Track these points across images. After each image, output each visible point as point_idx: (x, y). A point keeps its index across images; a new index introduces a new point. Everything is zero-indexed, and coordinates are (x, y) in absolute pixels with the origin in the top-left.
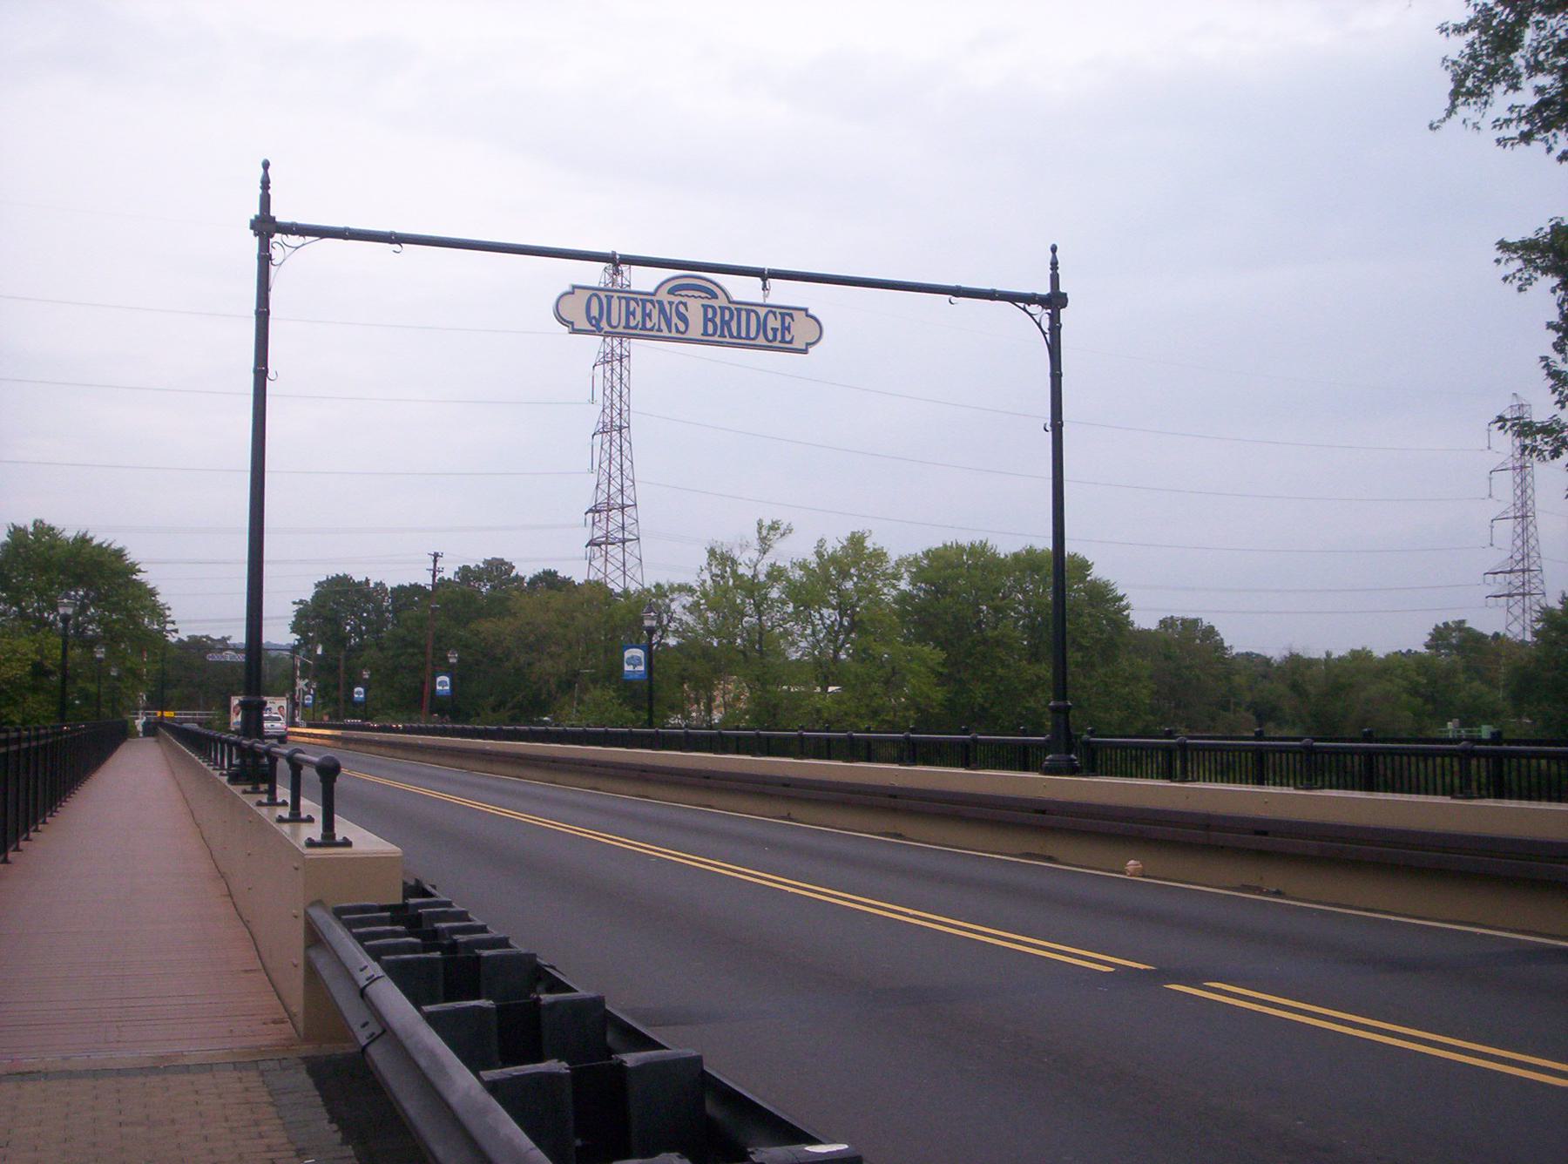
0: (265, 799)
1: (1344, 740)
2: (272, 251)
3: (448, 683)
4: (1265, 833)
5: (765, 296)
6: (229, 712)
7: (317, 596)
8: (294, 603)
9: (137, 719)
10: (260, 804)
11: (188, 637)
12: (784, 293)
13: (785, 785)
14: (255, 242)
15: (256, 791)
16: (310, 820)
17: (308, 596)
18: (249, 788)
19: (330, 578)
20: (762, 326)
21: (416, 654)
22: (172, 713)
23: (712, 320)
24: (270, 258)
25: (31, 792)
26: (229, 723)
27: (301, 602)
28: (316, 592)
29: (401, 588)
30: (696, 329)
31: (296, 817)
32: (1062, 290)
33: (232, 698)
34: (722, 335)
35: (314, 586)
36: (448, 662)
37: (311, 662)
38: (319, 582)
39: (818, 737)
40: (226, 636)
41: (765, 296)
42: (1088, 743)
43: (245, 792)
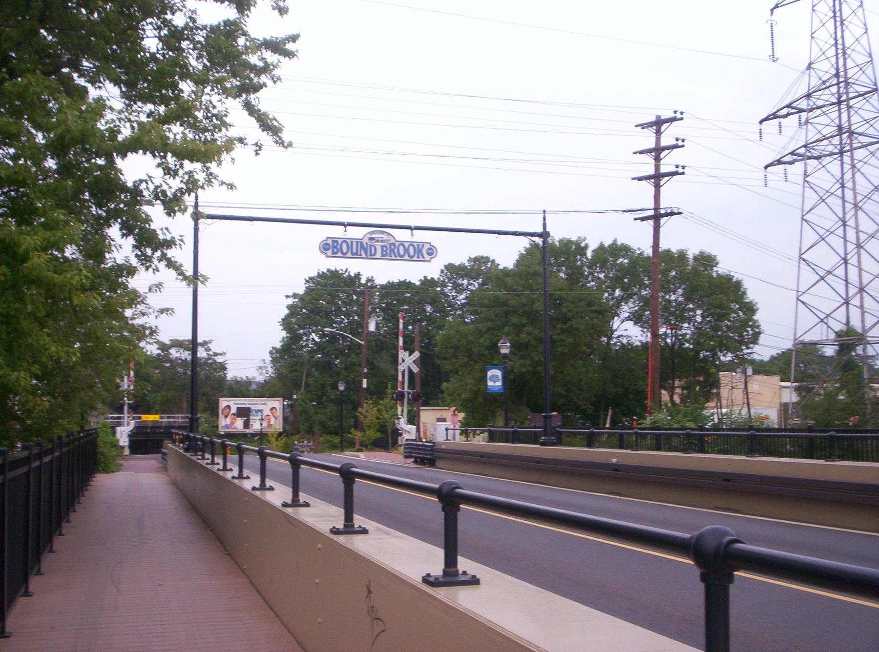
0: (200, 457)
1: (499, 428)
2: (200, 226)
3: (500, 378)
4: (617, 470)
5: (412, 238)
6: (217, 415)
7: (309, 291)
8: (287, 297)
9: (120, 424)
10: (199, 459)
11: (171, 340)
12: (420, 236)
13: (538, 462)
14: (192, 223)
15: (196, 455)
16: (218, 464)
17: (301, 290)
18: (193, 454)
19: (321, 272)
20: (406, 251)
21: (524, 326)
22: (157, 416)
23: (386, 251)
24: (198, 229)
25: (54, 475)
26: (217, 427)
27: (295, 296)
28: (307, 288)
29: (390, 285)
30: (379, 255)
31: (213, 463)
32: (548, 230)
33: (221, 399)
34: (391, 256)
35: (304, 282)
36: (500, 353)
37: (362, 343)
38: (310, 278)
39: (528, 432)
40: (207, 340)
41: (412, 238)
42: (558, 432)
43: (191, 455)
